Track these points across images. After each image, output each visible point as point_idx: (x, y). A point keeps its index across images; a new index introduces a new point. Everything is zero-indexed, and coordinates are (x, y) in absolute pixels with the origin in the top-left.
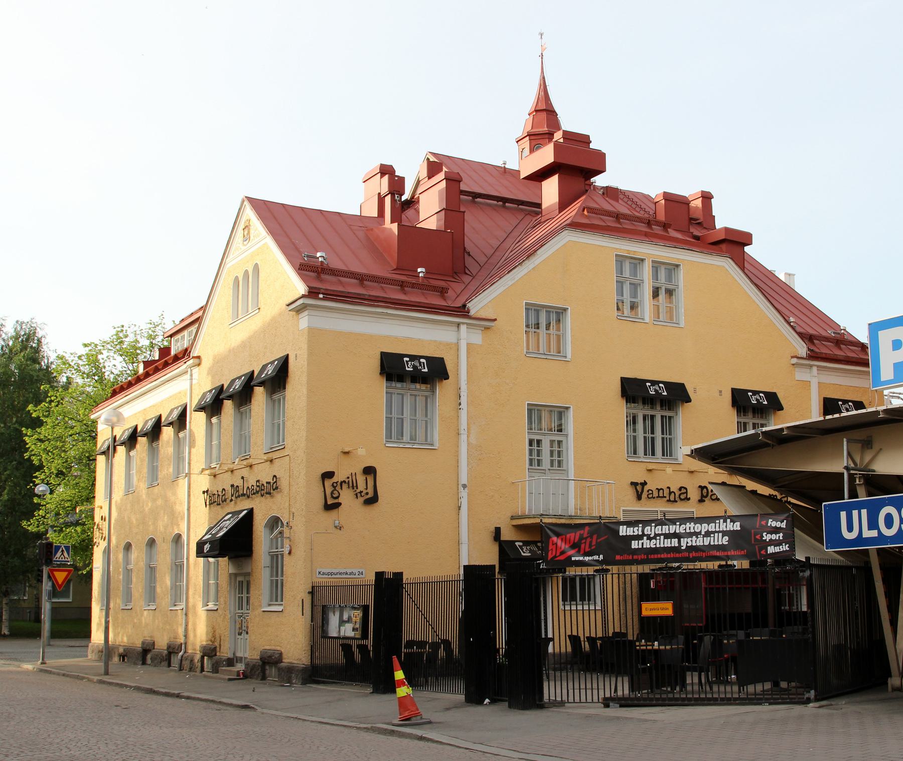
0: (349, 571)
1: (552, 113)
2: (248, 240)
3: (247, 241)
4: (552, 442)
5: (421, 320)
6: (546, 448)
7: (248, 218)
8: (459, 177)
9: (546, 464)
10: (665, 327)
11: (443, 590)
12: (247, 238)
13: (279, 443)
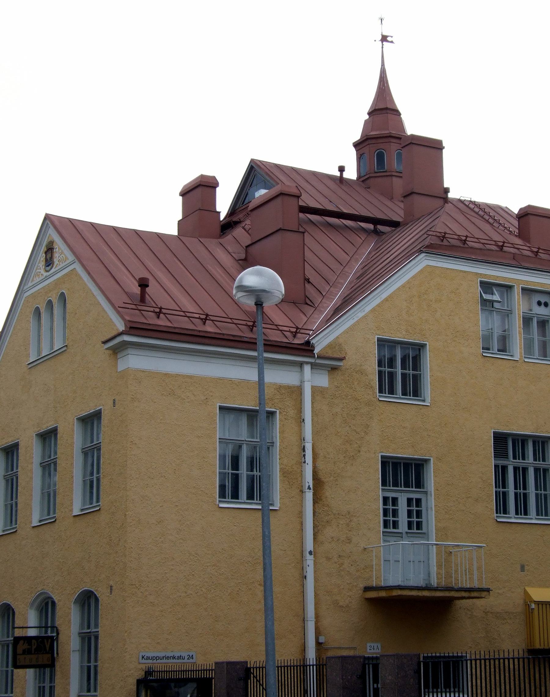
0: (177, 654)
1: (395, 113)
2: (51, 265)
3: (50, 267)
4: (409, 501)
5: (229, 355)
6: (403, 508)
7: (50, 239)
8: (298, 192)
9: (403, 526)
10: (505, 361)
11: (286, 676)
12: (49, 263)
13: (91, 504)
